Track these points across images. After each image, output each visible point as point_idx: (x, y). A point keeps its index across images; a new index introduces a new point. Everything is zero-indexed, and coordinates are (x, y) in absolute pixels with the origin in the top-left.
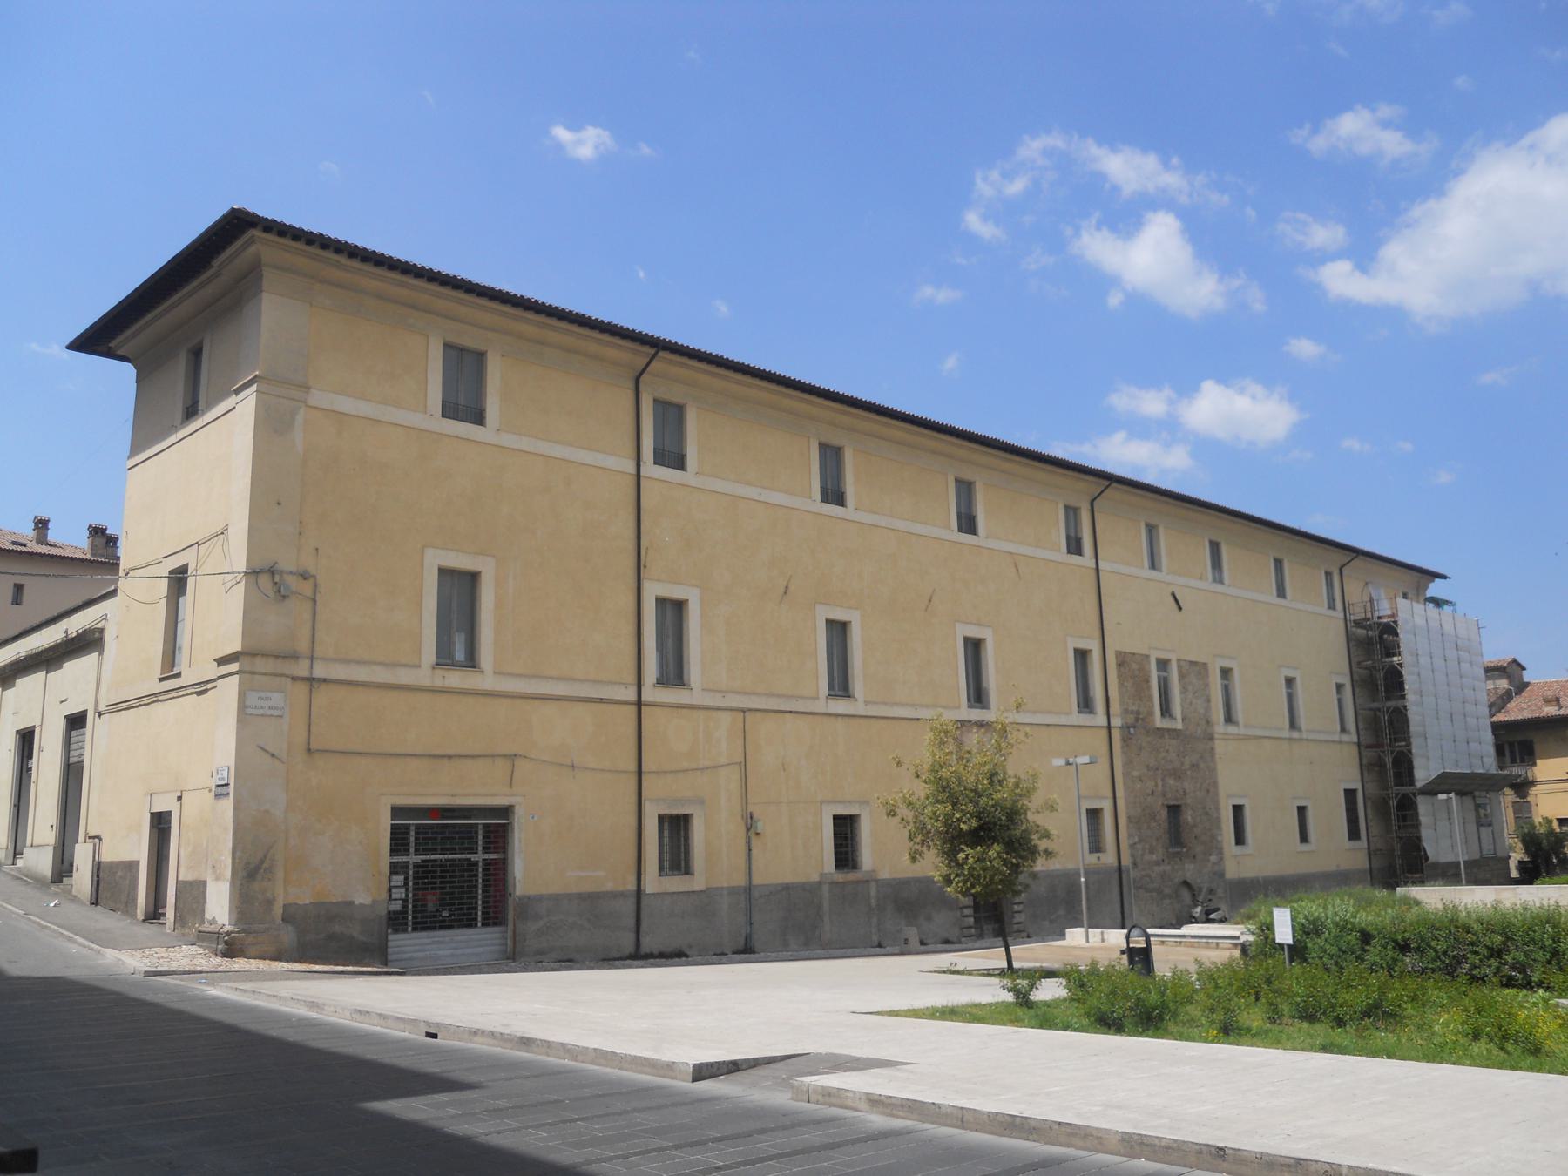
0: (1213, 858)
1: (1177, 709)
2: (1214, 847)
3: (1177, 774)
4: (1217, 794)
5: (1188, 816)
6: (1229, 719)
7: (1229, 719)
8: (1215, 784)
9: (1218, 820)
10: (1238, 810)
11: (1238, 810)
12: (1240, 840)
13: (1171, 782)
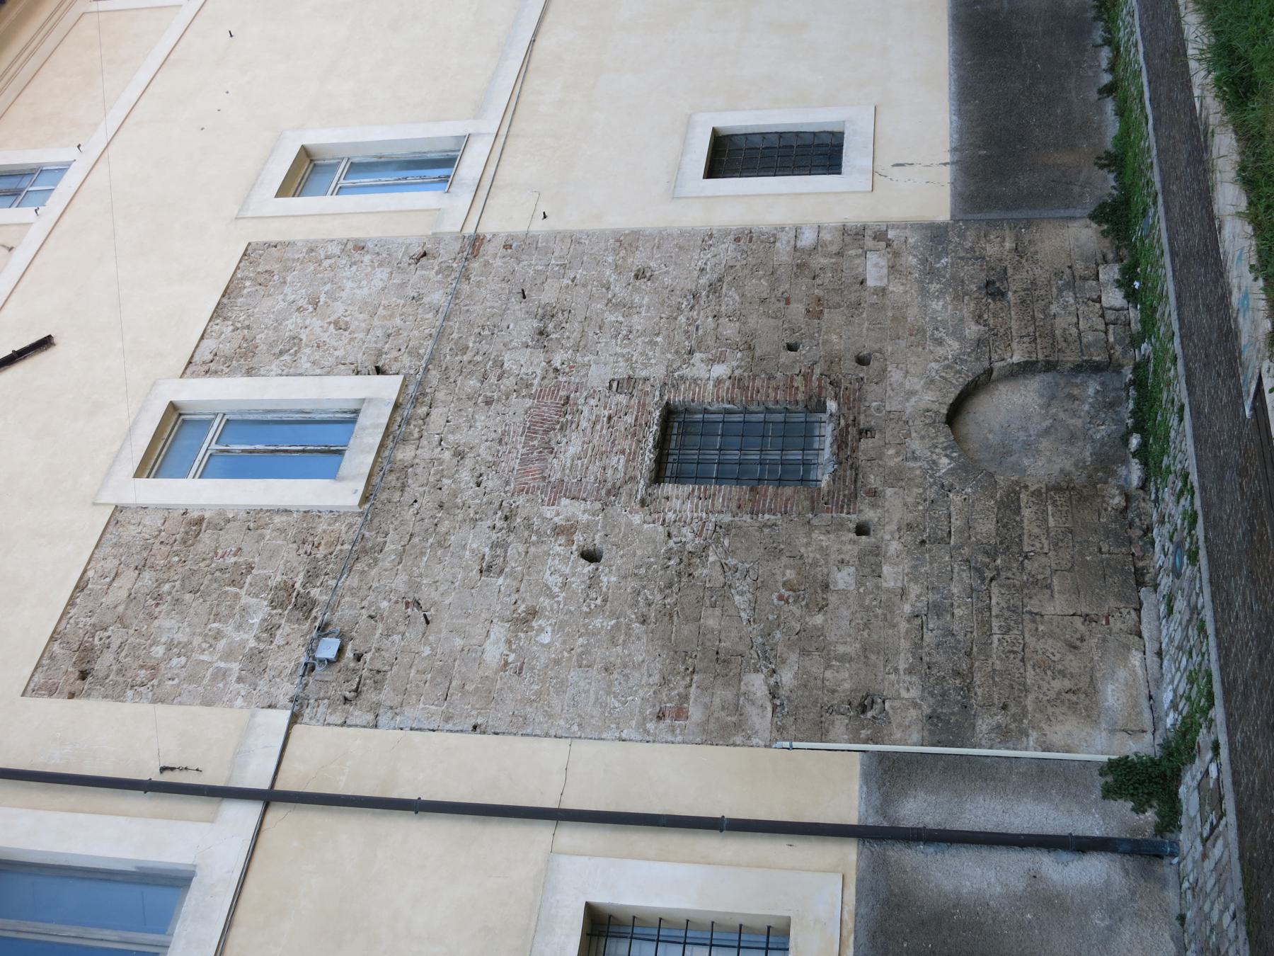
0: (874, 269)
1: (340, 390)
2: (820, 273)
3: (555, 412)
4: (658, 240)
5: (709, 378)
6: (436, 165)
7: (436, 165)
8: (626, 241)
9: (744, 237)
10: (729, 156)
11: (729, 156)
12: (817, 153)
13: (572, 446)
